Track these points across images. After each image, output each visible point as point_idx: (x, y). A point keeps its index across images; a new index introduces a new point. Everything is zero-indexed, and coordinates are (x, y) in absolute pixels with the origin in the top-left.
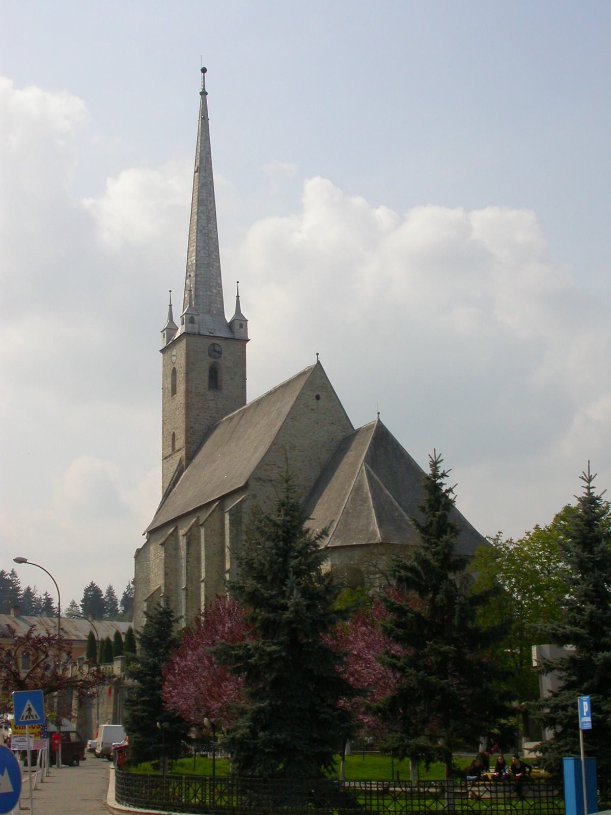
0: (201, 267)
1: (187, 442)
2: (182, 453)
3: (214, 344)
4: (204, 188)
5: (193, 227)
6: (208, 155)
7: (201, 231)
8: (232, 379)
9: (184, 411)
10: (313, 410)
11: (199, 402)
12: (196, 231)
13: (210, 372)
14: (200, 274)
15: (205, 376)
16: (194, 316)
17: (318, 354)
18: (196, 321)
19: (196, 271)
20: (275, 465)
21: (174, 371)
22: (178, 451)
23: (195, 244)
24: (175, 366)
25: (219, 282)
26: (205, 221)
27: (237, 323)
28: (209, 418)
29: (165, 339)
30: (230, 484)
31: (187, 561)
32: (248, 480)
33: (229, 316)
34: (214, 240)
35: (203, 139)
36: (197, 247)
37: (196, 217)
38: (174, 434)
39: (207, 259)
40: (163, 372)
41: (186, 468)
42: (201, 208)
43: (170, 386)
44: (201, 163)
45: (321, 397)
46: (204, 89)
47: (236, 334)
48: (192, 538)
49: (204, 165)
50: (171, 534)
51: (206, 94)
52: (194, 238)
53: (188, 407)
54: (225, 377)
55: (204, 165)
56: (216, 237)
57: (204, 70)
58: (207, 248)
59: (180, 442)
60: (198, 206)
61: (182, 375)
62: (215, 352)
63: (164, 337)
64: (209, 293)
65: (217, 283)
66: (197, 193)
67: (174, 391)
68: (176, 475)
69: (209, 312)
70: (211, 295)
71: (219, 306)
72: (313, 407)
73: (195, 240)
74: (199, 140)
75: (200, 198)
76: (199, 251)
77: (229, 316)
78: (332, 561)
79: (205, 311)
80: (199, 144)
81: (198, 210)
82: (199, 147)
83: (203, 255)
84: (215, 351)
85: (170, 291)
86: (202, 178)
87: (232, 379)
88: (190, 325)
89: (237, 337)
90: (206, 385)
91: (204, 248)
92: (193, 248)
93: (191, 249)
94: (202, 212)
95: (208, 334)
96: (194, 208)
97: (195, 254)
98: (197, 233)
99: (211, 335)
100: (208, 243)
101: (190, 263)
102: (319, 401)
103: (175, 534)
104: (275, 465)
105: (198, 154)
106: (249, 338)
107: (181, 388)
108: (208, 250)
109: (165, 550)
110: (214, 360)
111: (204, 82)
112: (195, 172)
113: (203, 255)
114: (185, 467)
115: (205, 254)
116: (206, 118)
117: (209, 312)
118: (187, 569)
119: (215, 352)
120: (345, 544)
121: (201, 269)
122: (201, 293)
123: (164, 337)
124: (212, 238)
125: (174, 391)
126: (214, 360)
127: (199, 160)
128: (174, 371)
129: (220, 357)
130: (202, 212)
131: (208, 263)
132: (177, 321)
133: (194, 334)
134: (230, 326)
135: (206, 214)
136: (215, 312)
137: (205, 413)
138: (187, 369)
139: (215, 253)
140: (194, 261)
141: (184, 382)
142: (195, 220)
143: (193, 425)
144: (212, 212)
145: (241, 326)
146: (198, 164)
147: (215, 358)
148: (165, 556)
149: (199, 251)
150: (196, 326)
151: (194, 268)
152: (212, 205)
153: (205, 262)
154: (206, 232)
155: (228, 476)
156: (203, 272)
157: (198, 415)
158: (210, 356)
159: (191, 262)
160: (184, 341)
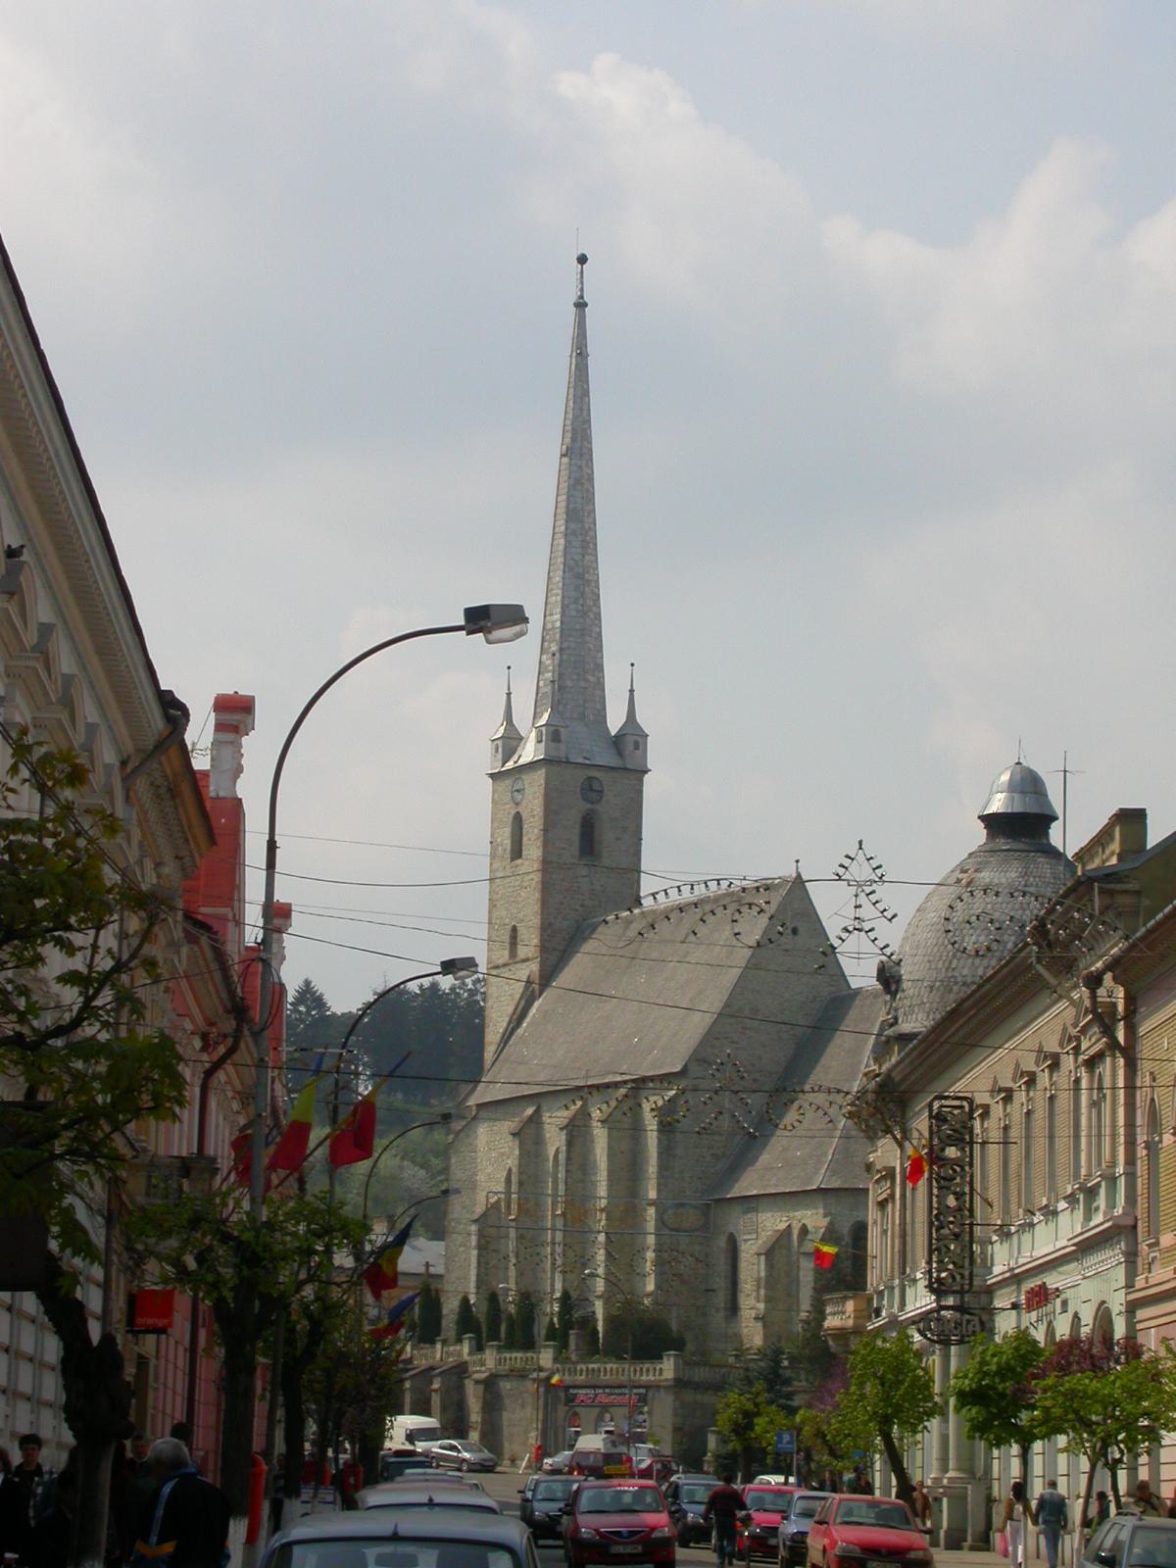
0: (570, 636)
1: (544, 948)
2: (534, 967)
3: (590, 779)
4: (579, 487)
5: (556, 558)
6: (586, 426)
7: (571, 569)
8: (618, 839)
9: (537, 895)
10: (786, 950)
11: (563, 880)
12: (562, 566)
13: (583, 826)
14: (569, 648)
15: (575, 835)
16: (561, 729)
17: (797, 861)
18: (563, 737)
19: (561, 643)
20: (726, 1038)
21: (518, 820)
22: (524, 961)
23: (560, 592)
24: (520, 809)
25: (599, 661)
26: (580, 551)
27: (630, 740)
28: (577, 907)
29: (500, 756)
30: (650, 1058)
31: (567, 1171)
32: (686, 1065)
33: (615, 722)
34: (593, 584)
35: (579, 393)
36: (563, 597)
37: (562, 541)
38: (514, 929)
39: (581, 620)
40: (494, 814)
41: (540, 996)
42: (572, 526)
43: (508, 843)
44: (574, 439)
45: (801, 930)
46: (582, 297)
47: (627, 755)
48: (576, 1131)
49: (578, 444)
50: (531, 1118)
51: (586, 305)
52: (557, 579)
53: (546, 888)
54: (607, 835)
55: (578, 444)
56: (595, 578)
57: (582, 260)
58: (581, 601)
59: (530, 942)
60: (567, 521)
61: (536, 831)
62: (591, 790)
63: (497, 751)
64: (582, 684)
65: (595, 664)
66: (565, 497)
67: (517, 852)
68: (521, 1006)
69: (582, 717)
70: (586, 688)
71: (598, 706)
72: (787, 947)
73: (561, 585)
74: (571, 396)
75: (571, 506)
76: (567, 606)
77: (615, 722)
78: (824, 1208)
79: (575, 715)
80: (571, 403)
81: (567, 529)
82: (570, 409)
83: (574, 613)
84: (591, 789)
85: (509, 668)
86: (575, 468)
87: (618, 839)
88: (553, 745)
89: (629, 766)
90: (575, 849)
91: (576, 601)
92: (556, 599)
93: (553, 599)
94: (574, 533)
95: (580, 760)
96: (558, 523)
97: (559, 610)
98: (564, 572)
99: (587, 762)
100: (583, 593)
101: (549, 626)
102: (796, 937)
103: (535, 1120)
104: (726, 1038)
105: (568, 422)
106: (649, 767)
107: (533, 851)
108: (583, 605)
109: (520, 1143)
110: (589, 806)
111: (582, 283)
112: (562, 456)
113: (574, 613)
114: (537, 992)
115: (578, 611)
116: (584, 353)
117: (582, 717)
118: (566, 1184)
119: (591, 790)
120: (847, 1186)
121: (571, 639)
122: (569, 683)
123: (497, 751)
124: (589, 582)
125: (517, 852)
126: (589, 806)
127: (569, 435)
128: (518, 820)
129: (600, 801)
130: (574, 533)
131: (583, 630)
132: (523, 720)
133: (559, 762)
134: (617, 742)
135: (580, 538)
136: (591, 717)
137: (572, 898)
138: (545, 823)
139: (595, 609)
140: (558, 624)
141: (539, 843)
142: (561, 548)
143: (553, 920)
144: (591, 533)
145: (637, 746)
146: (568, 440)
147: (592, 803)
148: (520, 1154)
149: (567, 606)
150: (563, 747)
151: (558, 636)
152: (591, 520)
153: (578, 626)
154: (581, 570)
155: (640, 1039)
156: (573, 645)
157: (562, 903)
158: (584, 799)
159: (553, 622)
160: (541, 773)
